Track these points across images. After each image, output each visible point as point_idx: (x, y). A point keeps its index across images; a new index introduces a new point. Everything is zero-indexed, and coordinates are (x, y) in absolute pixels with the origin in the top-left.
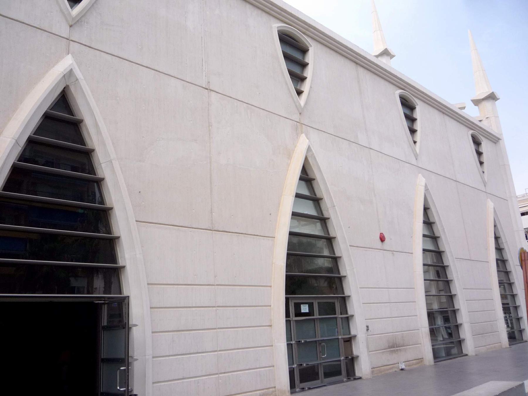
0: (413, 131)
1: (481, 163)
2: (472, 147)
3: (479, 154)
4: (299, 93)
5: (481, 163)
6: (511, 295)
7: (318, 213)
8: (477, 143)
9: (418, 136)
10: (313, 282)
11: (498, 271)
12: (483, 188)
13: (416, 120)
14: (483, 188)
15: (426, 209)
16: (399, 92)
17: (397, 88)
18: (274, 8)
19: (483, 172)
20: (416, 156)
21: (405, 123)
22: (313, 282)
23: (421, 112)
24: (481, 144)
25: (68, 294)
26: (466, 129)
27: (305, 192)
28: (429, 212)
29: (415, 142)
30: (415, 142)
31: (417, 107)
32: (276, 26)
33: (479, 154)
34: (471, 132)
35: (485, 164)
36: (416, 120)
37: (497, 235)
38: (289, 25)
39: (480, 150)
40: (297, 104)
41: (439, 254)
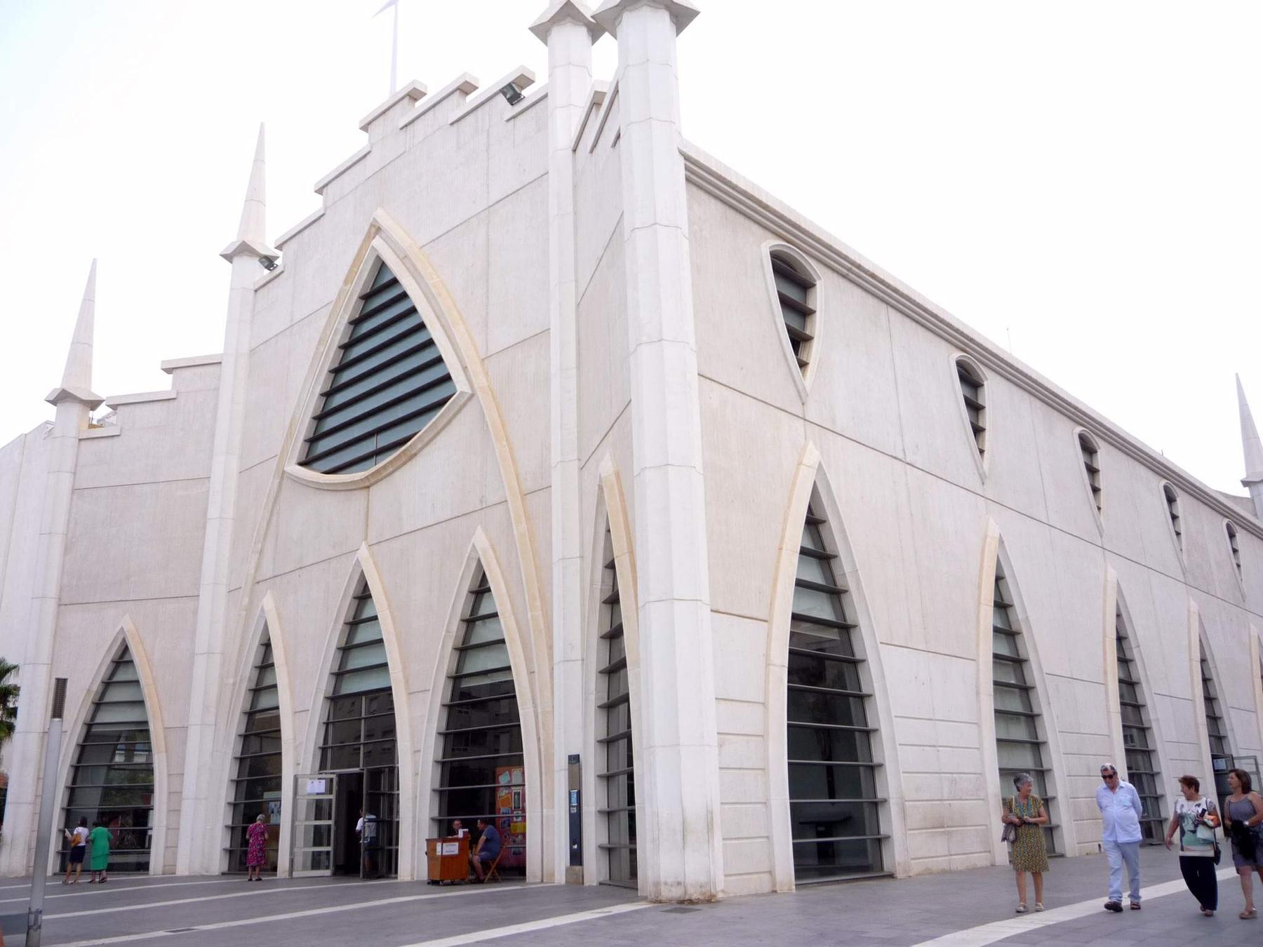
0: (978, 431)
1: (1096, 490)
3: (1092, 471)
4: (803, 365)
5: (1096, 490)
6: (1037, 771)
8: (1088, 449)
9: (815, 352)
10: (825, 696)
11: (1122, 704)
13: (812, 312)
15: (999, 579)
17: (953, 348)
19: (1099, 509)
20: (983, 479)
21: (779, 318)
22: (825, 696)
24: (1096, 452)
26: (1220, 517)
29: (982, 452)
30: (982, 452)
31: (818, 283)
33: (1092, 471)
34: (958, 354)
36: (812, 312)
37: (1122, 634)
39: (1095, 466)
40: (800, 387)
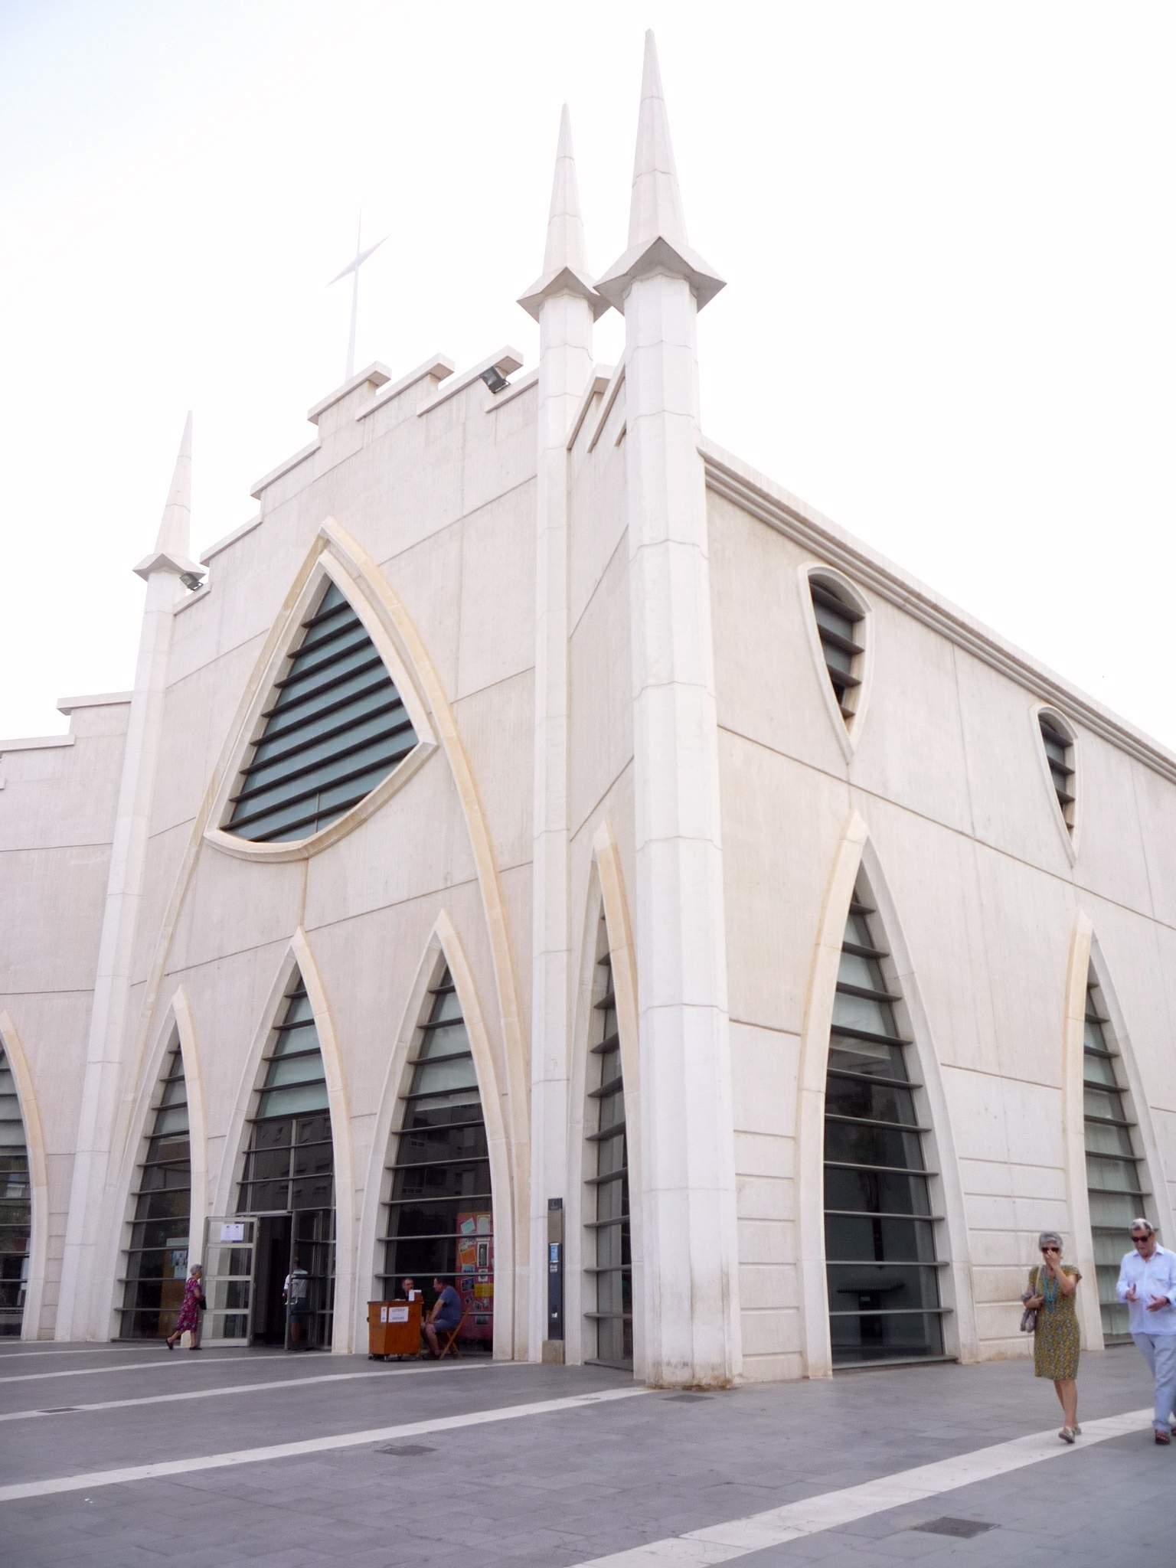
2: (1041, 751)
3: (1061, 772)
7: (887, 1030)
9: (862, 701)
12: (1063, 871)
13: (859, 651)
14: (1063, 871)
15: (1091, 987)
16: (1040, 706)
18: (922, 605)
21: (818, 657)
23: (879, 631)
25: (185, 1401)
27: (861, 979)
28: (1094, 992)
29: (1070, 827)
30: (1070, 827)
32: (808, 566)
35: (1077, 806)
36: (859, 651)
38: (831, 564)
41: (1115, 1093)
